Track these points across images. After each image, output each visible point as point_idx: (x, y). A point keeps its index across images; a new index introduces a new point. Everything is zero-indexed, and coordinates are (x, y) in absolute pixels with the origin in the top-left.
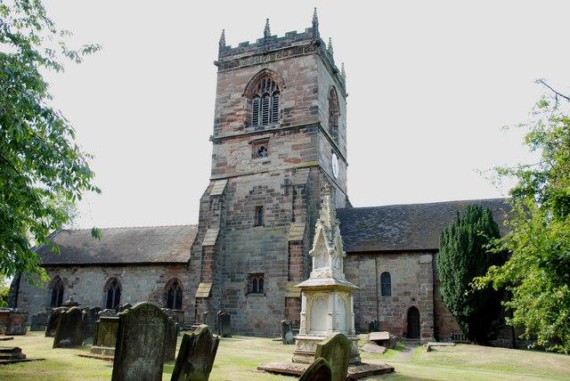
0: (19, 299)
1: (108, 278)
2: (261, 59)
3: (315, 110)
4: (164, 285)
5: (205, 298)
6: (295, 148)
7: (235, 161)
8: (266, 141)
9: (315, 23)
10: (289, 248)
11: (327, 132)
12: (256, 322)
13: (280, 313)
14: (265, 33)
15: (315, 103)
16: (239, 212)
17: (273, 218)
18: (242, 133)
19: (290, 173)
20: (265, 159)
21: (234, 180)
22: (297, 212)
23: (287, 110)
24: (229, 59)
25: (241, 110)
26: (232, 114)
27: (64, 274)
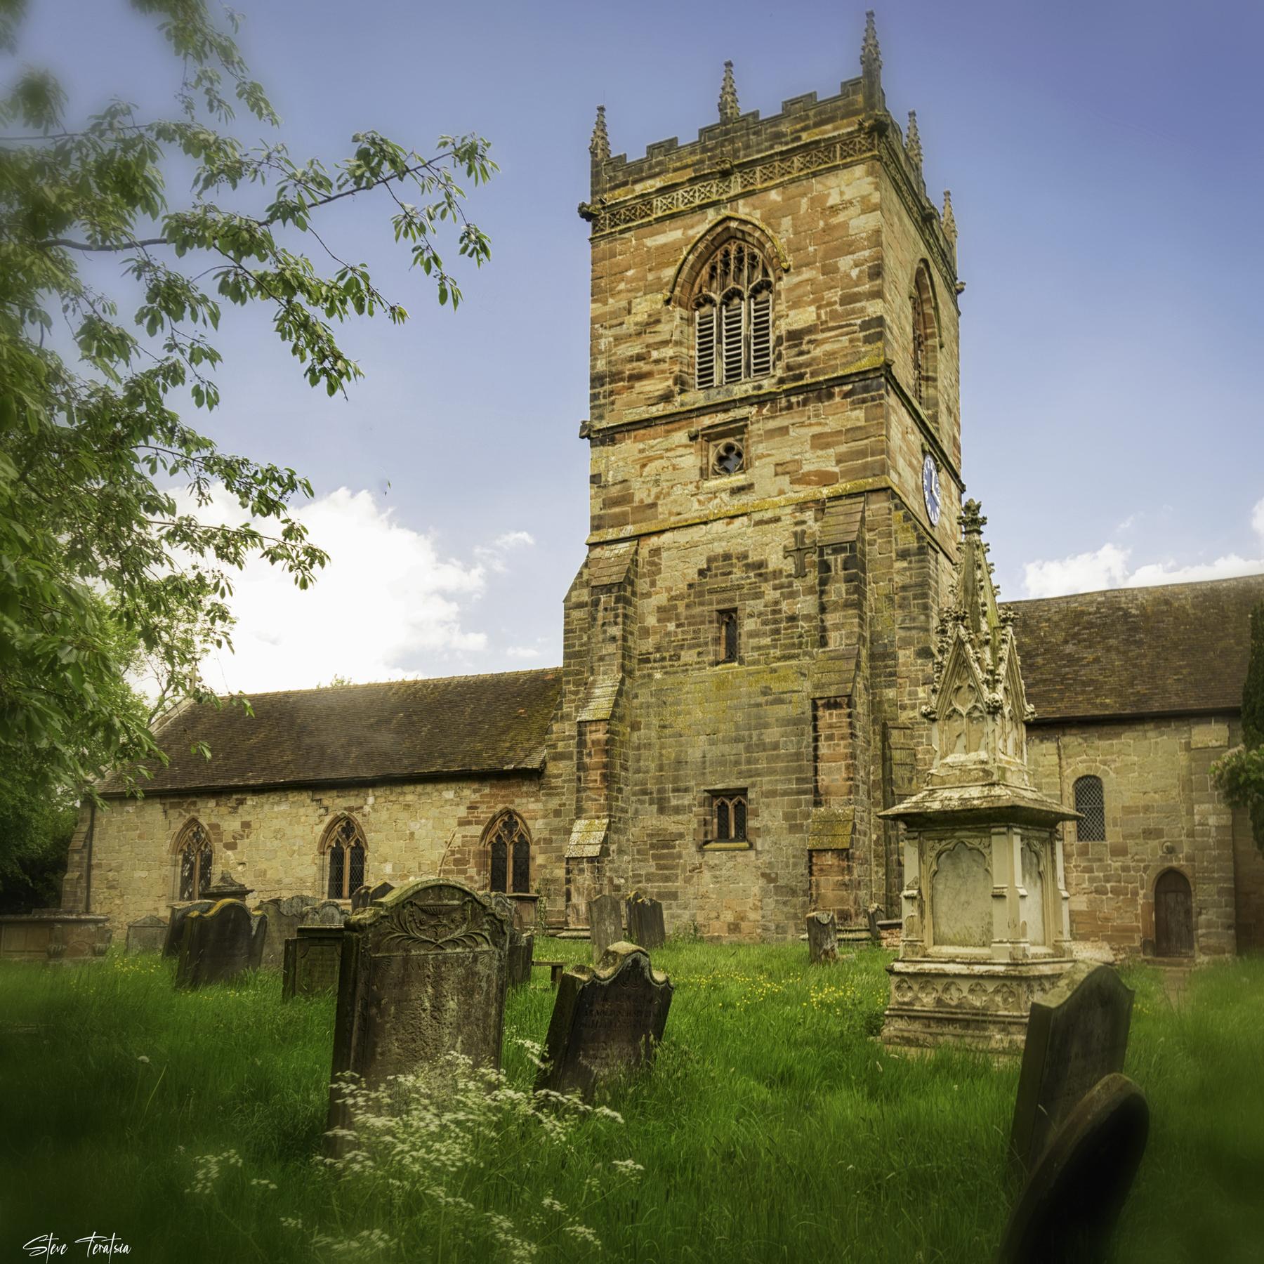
0: (95, 883)
1: (328, 819)
2: (714, 190)
3: (876, 329)
4: (478, 830)
5: (591, 859)
6: (820, 442)
7: (654, 491)
8: (739, 429)
9: (871, 65)
10: (815, 718)
11: (909, 394)
12: (729, 917)
13: (794, 892)
14: (722, 108)
15: (874, 308)
16: (671, 626)
17: (767, 641)
18: (670, 409)
19: (809, 515)
20: (738, 479)
21: (654, 541)
22: (831, 619)
23: (795, 337)
24: (620, 195)
25: (665, 343)
26: (640, 358)
27: (209, 813)
